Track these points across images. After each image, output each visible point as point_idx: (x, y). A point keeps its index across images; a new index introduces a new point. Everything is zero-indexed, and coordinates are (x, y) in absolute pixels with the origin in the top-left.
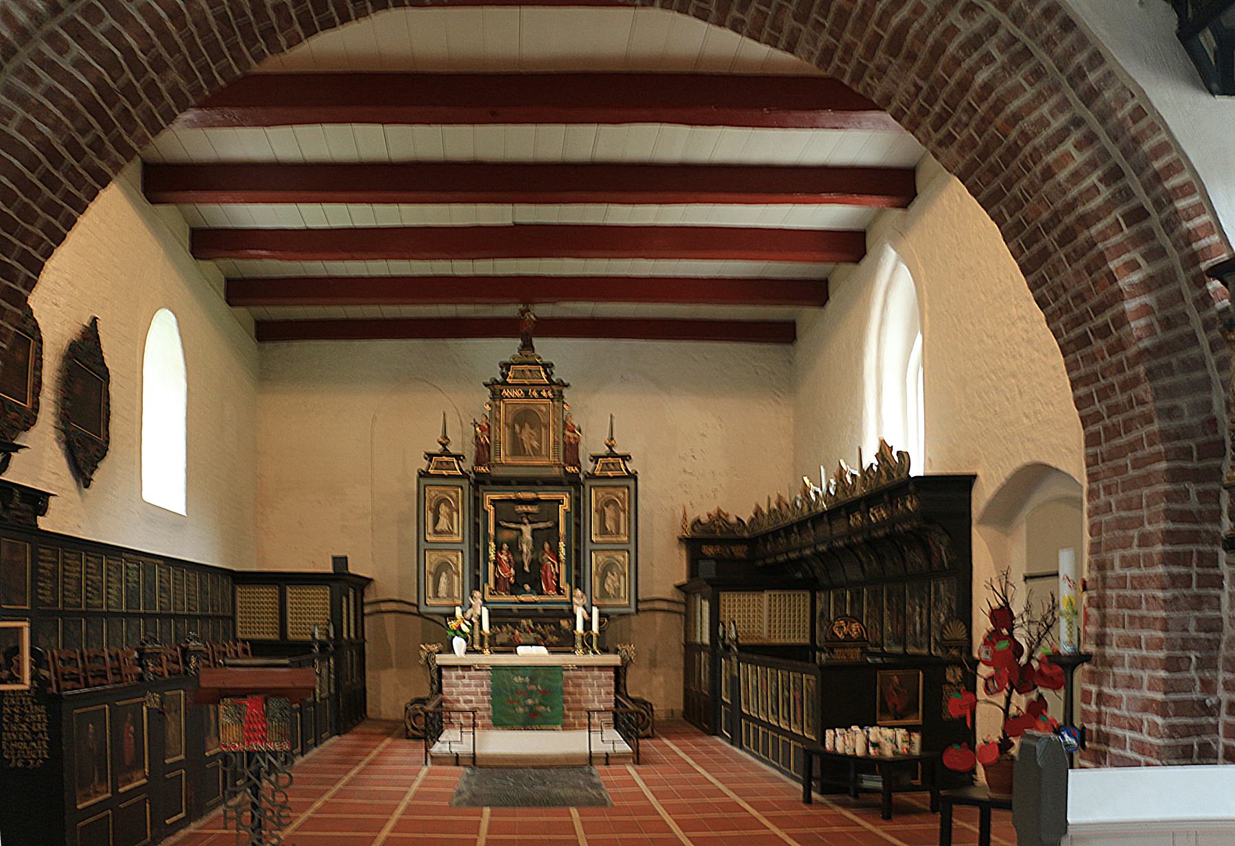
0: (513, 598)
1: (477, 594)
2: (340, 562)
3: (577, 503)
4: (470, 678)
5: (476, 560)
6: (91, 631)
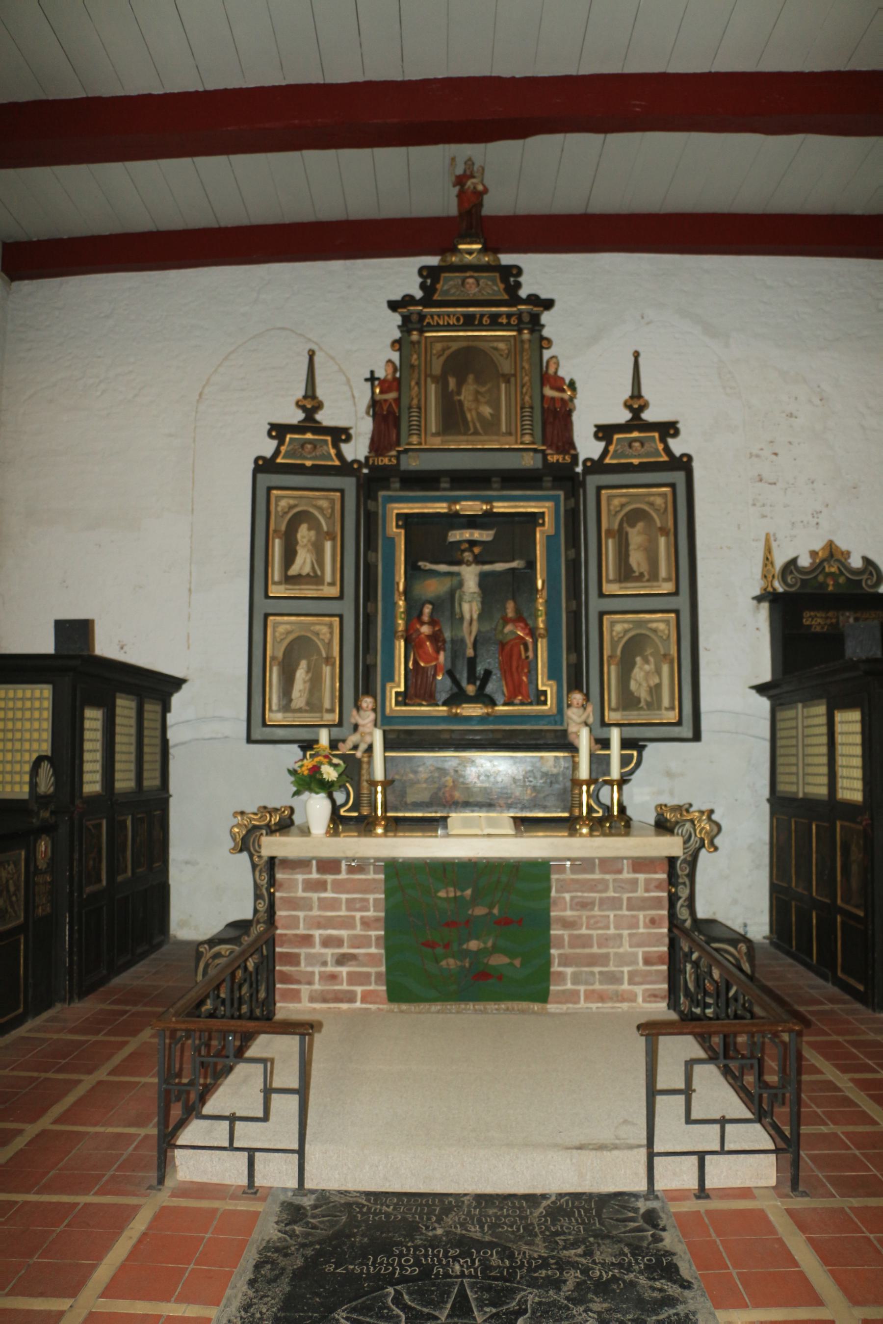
1: (367, 702)
2: (75, 633)
3: (572, 522)
4: (339, 887)
6: (390, 798)
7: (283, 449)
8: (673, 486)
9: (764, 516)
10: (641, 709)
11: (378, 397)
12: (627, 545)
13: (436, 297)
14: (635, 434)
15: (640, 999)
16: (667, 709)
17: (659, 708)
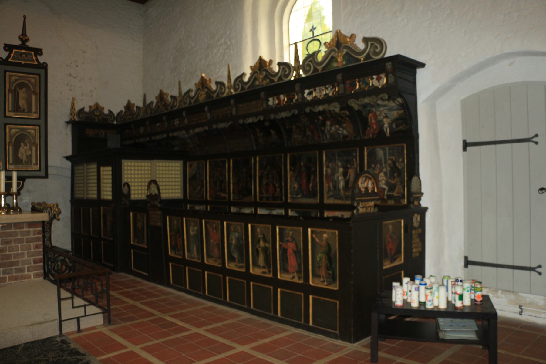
8: (39, 75)
9: (71, 90)
10: (23, 164)
12: (18, 97)
14: (23, 51)
15: (32, 277)
16: (34, 164)
17: (31, 164)
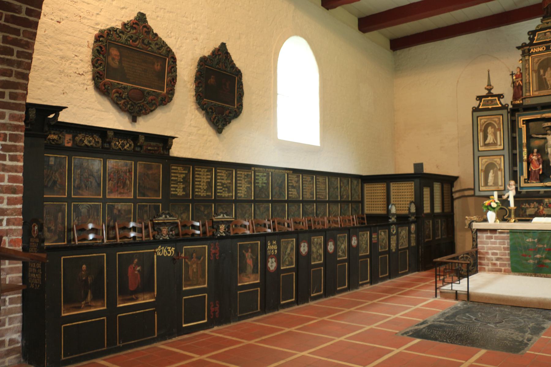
0: (541, 184)
2: (419, 166)
4: (496, 238)
5: (514, 160)
7: (481, 104)
11: (514, 80)
13: (534, 42)
14: (490, 98)
